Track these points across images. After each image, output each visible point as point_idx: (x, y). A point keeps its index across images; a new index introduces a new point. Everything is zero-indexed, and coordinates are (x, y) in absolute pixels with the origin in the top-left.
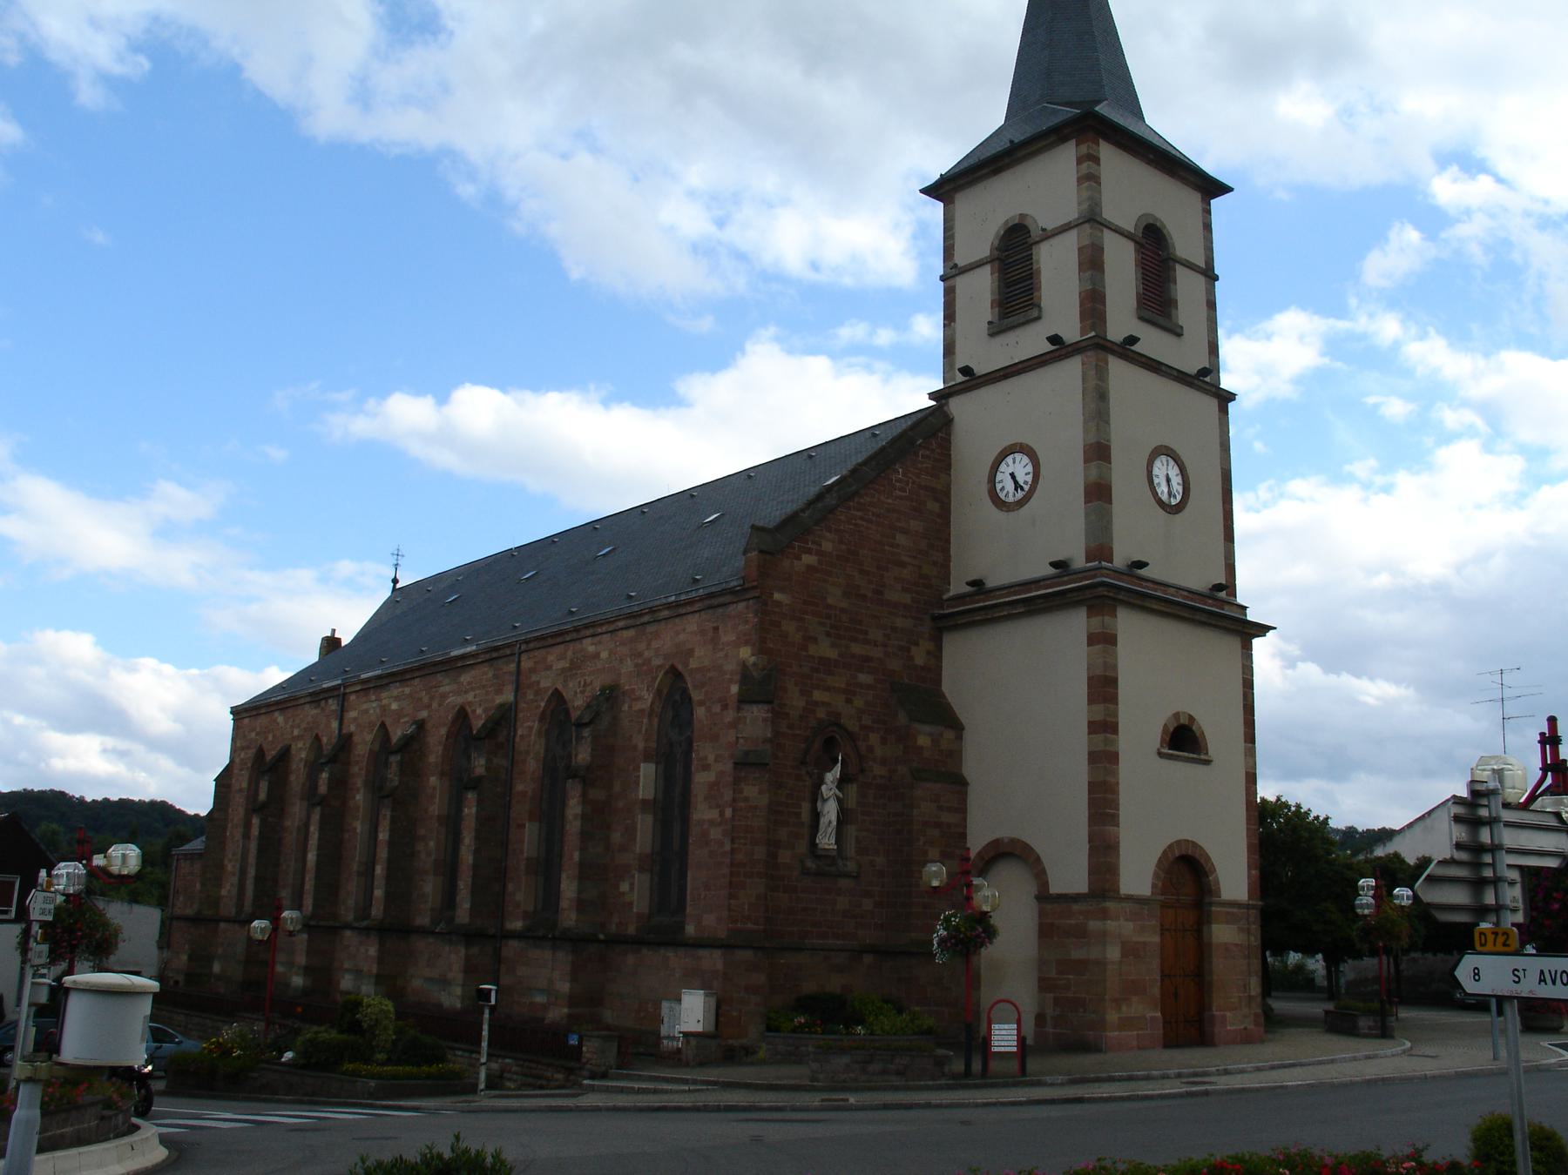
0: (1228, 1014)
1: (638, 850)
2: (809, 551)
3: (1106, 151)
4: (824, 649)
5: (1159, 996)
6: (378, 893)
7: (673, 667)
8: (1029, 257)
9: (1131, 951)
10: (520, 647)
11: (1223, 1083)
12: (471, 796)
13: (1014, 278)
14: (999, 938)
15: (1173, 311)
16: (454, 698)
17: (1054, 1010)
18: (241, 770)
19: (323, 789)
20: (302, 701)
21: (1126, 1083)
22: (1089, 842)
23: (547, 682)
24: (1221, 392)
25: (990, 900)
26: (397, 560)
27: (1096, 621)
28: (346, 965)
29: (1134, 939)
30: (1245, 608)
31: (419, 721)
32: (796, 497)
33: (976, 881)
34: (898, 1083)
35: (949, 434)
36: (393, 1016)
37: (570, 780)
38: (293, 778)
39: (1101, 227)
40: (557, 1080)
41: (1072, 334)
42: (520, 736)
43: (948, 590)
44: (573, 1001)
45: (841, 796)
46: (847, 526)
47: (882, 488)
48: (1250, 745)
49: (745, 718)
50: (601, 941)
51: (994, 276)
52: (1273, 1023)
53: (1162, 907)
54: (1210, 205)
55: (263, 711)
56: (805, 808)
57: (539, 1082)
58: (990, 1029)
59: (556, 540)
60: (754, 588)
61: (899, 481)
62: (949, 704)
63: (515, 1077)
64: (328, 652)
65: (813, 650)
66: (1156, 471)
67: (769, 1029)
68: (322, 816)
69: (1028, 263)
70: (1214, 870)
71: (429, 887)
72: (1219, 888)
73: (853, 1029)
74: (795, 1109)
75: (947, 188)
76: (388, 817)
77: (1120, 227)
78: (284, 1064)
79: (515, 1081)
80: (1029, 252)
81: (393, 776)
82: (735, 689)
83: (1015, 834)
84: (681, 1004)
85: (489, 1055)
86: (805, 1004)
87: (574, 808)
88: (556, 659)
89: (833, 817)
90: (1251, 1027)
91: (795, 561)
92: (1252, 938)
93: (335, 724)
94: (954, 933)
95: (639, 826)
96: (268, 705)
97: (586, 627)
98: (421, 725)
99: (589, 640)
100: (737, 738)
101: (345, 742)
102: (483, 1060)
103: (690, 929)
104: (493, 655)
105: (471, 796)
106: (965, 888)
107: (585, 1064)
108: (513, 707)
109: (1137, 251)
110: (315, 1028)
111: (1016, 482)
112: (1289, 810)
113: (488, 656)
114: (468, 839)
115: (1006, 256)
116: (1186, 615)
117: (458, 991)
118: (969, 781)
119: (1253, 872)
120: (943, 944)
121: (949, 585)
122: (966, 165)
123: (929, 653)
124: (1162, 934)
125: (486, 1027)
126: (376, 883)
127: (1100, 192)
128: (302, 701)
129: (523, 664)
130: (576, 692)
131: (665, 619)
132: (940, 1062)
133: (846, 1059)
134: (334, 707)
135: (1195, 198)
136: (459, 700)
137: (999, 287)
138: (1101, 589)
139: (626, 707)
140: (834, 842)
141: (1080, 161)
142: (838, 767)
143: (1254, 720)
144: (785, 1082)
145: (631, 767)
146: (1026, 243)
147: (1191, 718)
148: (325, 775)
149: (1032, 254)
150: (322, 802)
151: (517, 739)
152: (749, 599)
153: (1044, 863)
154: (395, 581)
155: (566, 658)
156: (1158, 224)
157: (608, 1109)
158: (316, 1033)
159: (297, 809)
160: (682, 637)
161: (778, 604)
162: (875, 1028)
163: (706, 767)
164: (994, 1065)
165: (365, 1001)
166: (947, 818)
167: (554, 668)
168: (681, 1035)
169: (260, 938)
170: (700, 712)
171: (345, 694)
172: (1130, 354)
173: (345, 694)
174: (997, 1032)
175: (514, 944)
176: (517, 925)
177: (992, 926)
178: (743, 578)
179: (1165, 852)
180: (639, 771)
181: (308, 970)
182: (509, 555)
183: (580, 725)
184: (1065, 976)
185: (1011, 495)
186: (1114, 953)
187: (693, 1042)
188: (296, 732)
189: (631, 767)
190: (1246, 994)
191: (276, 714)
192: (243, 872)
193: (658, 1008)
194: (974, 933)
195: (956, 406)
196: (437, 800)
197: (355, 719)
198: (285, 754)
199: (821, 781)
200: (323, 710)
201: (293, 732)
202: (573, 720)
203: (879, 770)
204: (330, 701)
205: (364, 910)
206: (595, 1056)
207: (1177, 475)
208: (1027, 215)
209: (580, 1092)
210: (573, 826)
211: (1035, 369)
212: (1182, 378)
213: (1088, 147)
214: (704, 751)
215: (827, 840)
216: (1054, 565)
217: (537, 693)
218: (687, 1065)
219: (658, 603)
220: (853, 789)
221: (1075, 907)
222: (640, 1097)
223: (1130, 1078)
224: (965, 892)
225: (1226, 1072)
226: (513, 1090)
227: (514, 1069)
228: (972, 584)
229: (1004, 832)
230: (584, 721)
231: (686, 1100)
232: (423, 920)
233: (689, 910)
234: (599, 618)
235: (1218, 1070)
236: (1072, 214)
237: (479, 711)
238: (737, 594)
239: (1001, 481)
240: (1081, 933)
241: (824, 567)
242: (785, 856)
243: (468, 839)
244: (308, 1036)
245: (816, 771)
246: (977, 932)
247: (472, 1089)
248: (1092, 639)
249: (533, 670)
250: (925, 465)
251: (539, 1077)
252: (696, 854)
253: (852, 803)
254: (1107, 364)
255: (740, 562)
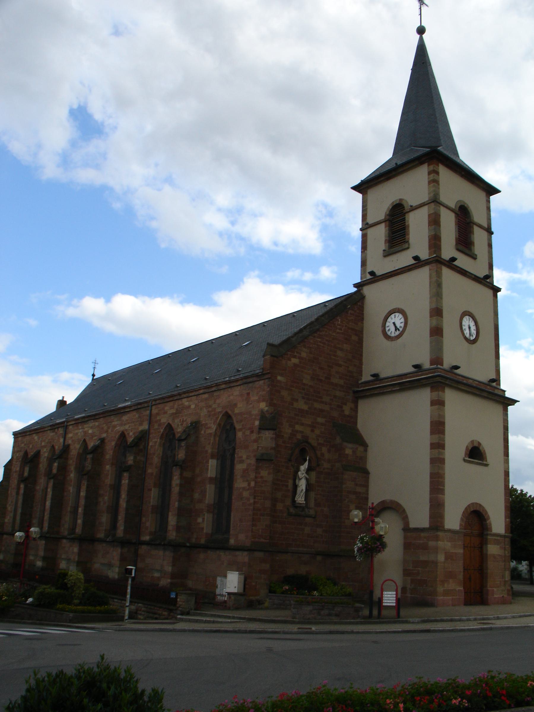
0: (495, 589)
1: (207, 502)
2: (295, 357)
3: (443, 170)
4: (302, 405)
5: (462, 579)
6: (80, 521)
7: (227, 412)
8: (404, 219)
9: (449, 557)
10: (152, 403)
11: (499, 624)
12: (126, 474)
13: (395, 230)
14: (387, 548)
15: (472, 247)
16: (119, 427)
17: (411, 585)
18: (17, 462)
19: (55, 471)
20: (46, 429)
21: (450, 623)
22: (430, 502)
23: (164, 420)
24: (495, 287)
25: (384, 529)
26: (95, 365)
27: (435, 394)
28: (63, 557)
29: (451, 551)
30: (505, 391)
31: (102, 438)
32: (287, 334)
33: (377, 520)
34: (336, 620)
35: (363, 303)
36: (83, 581)
37: (175, 467)
38: (41, 466)
39: (438, 205)
40: (164, 615)
41: (424, 255)
42: (151, 446)
43: (361, 379)
44: (173, 576)
45: (308, 477)
46: (314, 346)
47: (331, 328)
48: (507, 458)
49: (262, 437)
50: (188, 547)
51: (386, 228)
52: (515, 595)
53: (465, 535)
54: (489, 198)
55: (28, 434)
56: (290, 483)
57: (155, 616)
58: (382, 594)
59: (170, 356)
60: (269, 373)
61: (339, 325)
62: (361, 434)
63: (143, 613)
64: (60, 407)
65: (295, 405)
66: (463, 323)
67: (270, 592)
68: (54, 484)
69: (403, 222)
70: (489, 518)
71: (104, 519)
72: (491, 527)
73: (312, 592)
74: (285, 633)
75: (364, 187)
76: (86, 484)
77: (448, 206)
78: (28, 604)
79: (144, 615)
80: (404, 217)
81: (88, 465)
82: (257, 423)
83: (393, 498)
84: (226, 578)
85: (131, 602)
86: (289, 580)
87: (176, 481)
88: (169, 409)
89: (304, 488)
90: (505, 596)
91: (288, 361)
92: (507, 552)
93: (62, 440)
94: (365, 545)
95: (208, 490)
96: (30, 431)
97: (184, 393)
98: (103, 441)
99: (185, 399)
100: (258, 447)
101: (66, 449)
102: (128, 604)
103: (232, 541)
104: (138, 407)
105: (126, 474)
106: (371, 523)
107: (179, 607)
108: (148, 432)
109: (456, 217)
110: (45, 586)
111: (396, 327)
112: (517, 493)
113: (136, 407)
114: (124, 496)
115: (393, 219)
116: (478, 393)
117: (117, 570)
118: (370, 472)
119: (507, 520)
120: (360, 551)
121: (362, 376)
122: (373, 175)
123: (351, 409)
124: (464, 549)
125: (129, 588)
126: (78, 517)
127: (439, 188)
128: (46, 429)
129: (153, 411)
130: (178, 425)
131: (223, 389)
132: (357, 610)
133: (310, 608)
134: (61, 432)
135: (482, 194)
136: (122, 429)
137: (389, 234)
138: (438, 378)
139: (203, 432)
140: (304, 499)
141: (429, 173)
142: (307, 463)
143: (508, 446)
144: (279, 619)
145: (204, 462)
146: (402, 213)
147: (479, 444)
148: (56, 464)
149: (405, 218)
150: (54, 477)
151: (149, 447)
152: (265, 379)
153: (407, 512)
154: (93, 375)
155: (174, 408)
156: (466, 205)
157: (189, 631)
158: (44, 589)
159: (42, 481)
160: (231, 397)
161: (280, 382)
162: (323, 592)
163: (242, 462)
164: (384, 612)
165: (70, 573)
166: (359, 489)
167: (168, 413)
168: (227, 594)
169: (19, 541)
170: (239, 435)
171: (67, 426)
172: (453, 266)
173: (67, 426)
174: (386, 596)
175: (144, 547)
176: (147, 538)
177: (385, 542)
178: (263, 369)
179: (466, 509)
180: (209, 463)
181: (44, 559)
182: (148, 363)
183: (180, 440)
184: (417, 569)
185: (393, 333)
186: (441, 558)
187: (233, 597)
188: (43, 444)
189: (204, 462)
190: (504, 580)
191: (34, 435)
192: (15, 511)
193: (215, 580)
194: (375, 546)
195: (366, 290)
196: (109, 477)
197: (72, 437)
198: (37, 455)
199: (298, 470)
200: (56, 433)
201: (41, 444)
202: (176, 438)
203: (326, 465)
204: (60, 429)
205: (72, 530)
206: (184, 604)
207: (474, 326)
208: (403, 199)
209: (176, 621)
210: (175, 489)
211: (406, 272)
212: (476, 279)
213: (434, 167)
214: (241, 453)
215: (300, 499)
216: (415, 366)
217: (160, 425)
218: (229, 609)
219: (220, 381)
220: (313, 474)
221: (422, 534)
222: (206, 625)
223: (451, 620)
224: (371, 525)
225: (498, 618)
226: (142, 619)
227: (143, 609)
228: (373, 376)
229: (387, 497)
230: (183, 438)
231: (229, 627)
232: (101, 535)
233: (232, 532)
234: (191, 388)
235: (494, 617)
236: (425, 198)
237: (131, 434)
238: (259, 376)
239: (388, 326)
240: (425, 547)
241: (302, 365)
242: (280, 506)
243: (124, 496)
244: (40, 590)
245: (296, 465)
246: (377, 545)
247: (121, 619)
248: (433, 403)
249: (158, 414)
250: (351, 318)
251: (155, 613)
252: (236, 504)
253: (313, 481)
254: (441, 270)
255: (261, 362)
